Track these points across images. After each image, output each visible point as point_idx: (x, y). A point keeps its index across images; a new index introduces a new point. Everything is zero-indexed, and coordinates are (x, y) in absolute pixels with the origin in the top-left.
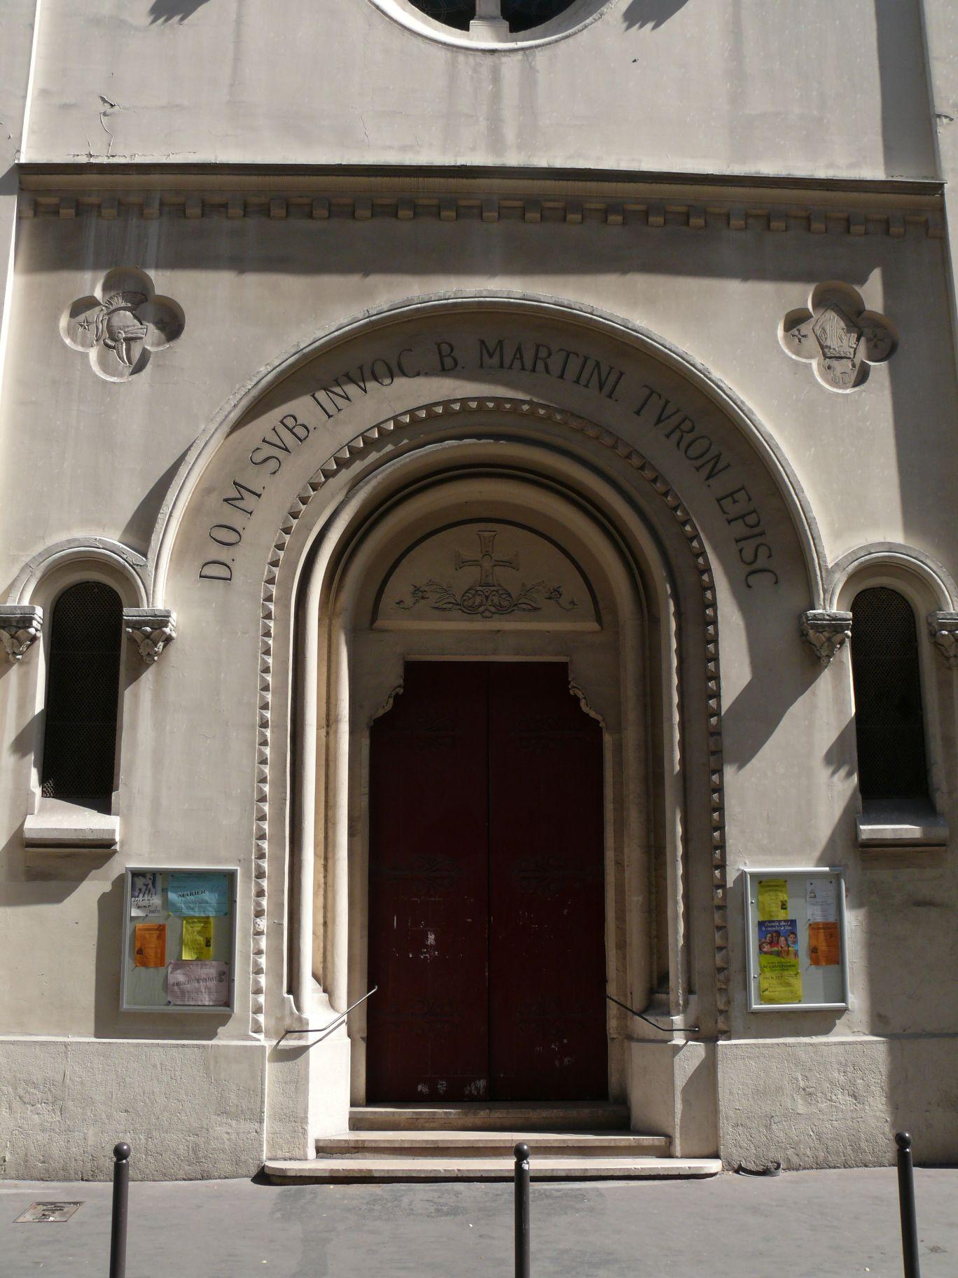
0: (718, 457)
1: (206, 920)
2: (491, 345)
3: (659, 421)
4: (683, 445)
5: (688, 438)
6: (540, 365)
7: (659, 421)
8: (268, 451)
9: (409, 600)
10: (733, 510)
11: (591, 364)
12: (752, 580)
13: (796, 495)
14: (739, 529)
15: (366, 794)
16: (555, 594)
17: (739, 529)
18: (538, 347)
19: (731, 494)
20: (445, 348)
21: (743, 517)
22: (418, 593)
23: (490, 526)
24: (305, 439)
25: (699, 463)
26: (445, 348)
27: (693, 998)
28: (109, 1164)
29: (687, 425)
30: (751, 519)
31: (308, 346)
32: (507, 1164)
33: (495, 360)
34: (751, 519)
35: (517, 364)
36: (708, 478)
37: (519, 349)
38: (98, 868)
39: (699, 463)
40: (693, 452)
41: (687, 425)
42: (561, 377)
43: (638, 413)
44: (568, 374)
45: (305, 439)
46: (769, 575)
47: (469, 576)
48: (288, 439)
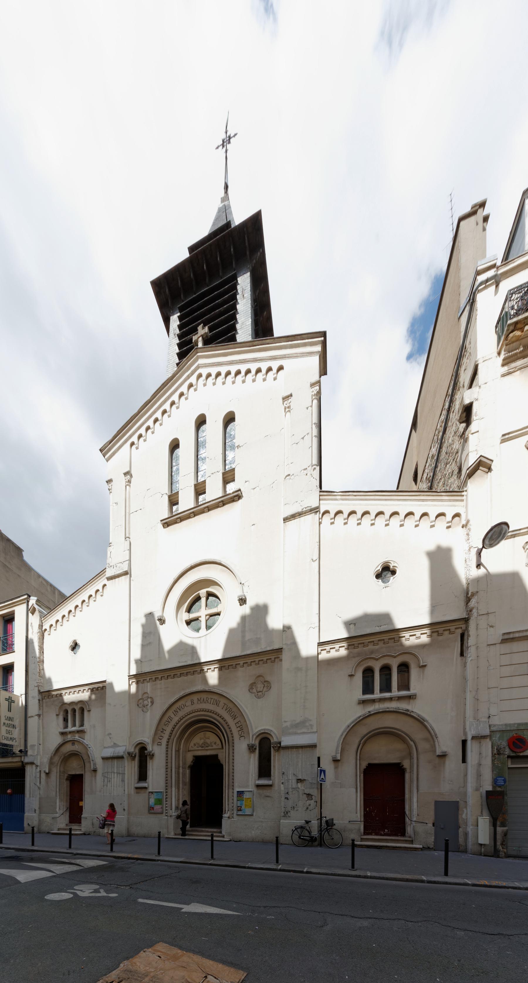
0: (236, 715)
1: (126, 746)
2: (199, 699)
3: (226, 710)
4: (230, 714)
5: (231, 712)
6: (207, 702)
7: (226, 710)
8: (167, 723)
9: (193, 746)
10: (238, 725)
11: (215, 700)
12: (241, 738)
13: (56, 785)
14: (239, 729)
15: (30, 717)
16: (215, 743)
17: (239, 729)
18: (207, 698)
19: (238, 722)
20: (192, 701)
21: (239, 726)
22: (195, 745)
23: (205, 732)
24: (315, 561)
25: (232, 717)
26: (192, 701)
27: (229, 812)
28: (157, 836)
29: (231, 710)
30: (241, 727)
31: (211, 632)
32: (68, 832)
33: (200, 702)
34: (241, 727)
35: (203, 702)
36: (234, 719)
37: (204, 699)
38: (188, 905)
39: (232, 717)
40: (232, 715)
41: (231, 710)
42: (210, 703)
43: (222, 709)
44: (212, 703)
45: (315, 561)
46: (244, 737)
47: (202, 741)
48: (170, 720)
